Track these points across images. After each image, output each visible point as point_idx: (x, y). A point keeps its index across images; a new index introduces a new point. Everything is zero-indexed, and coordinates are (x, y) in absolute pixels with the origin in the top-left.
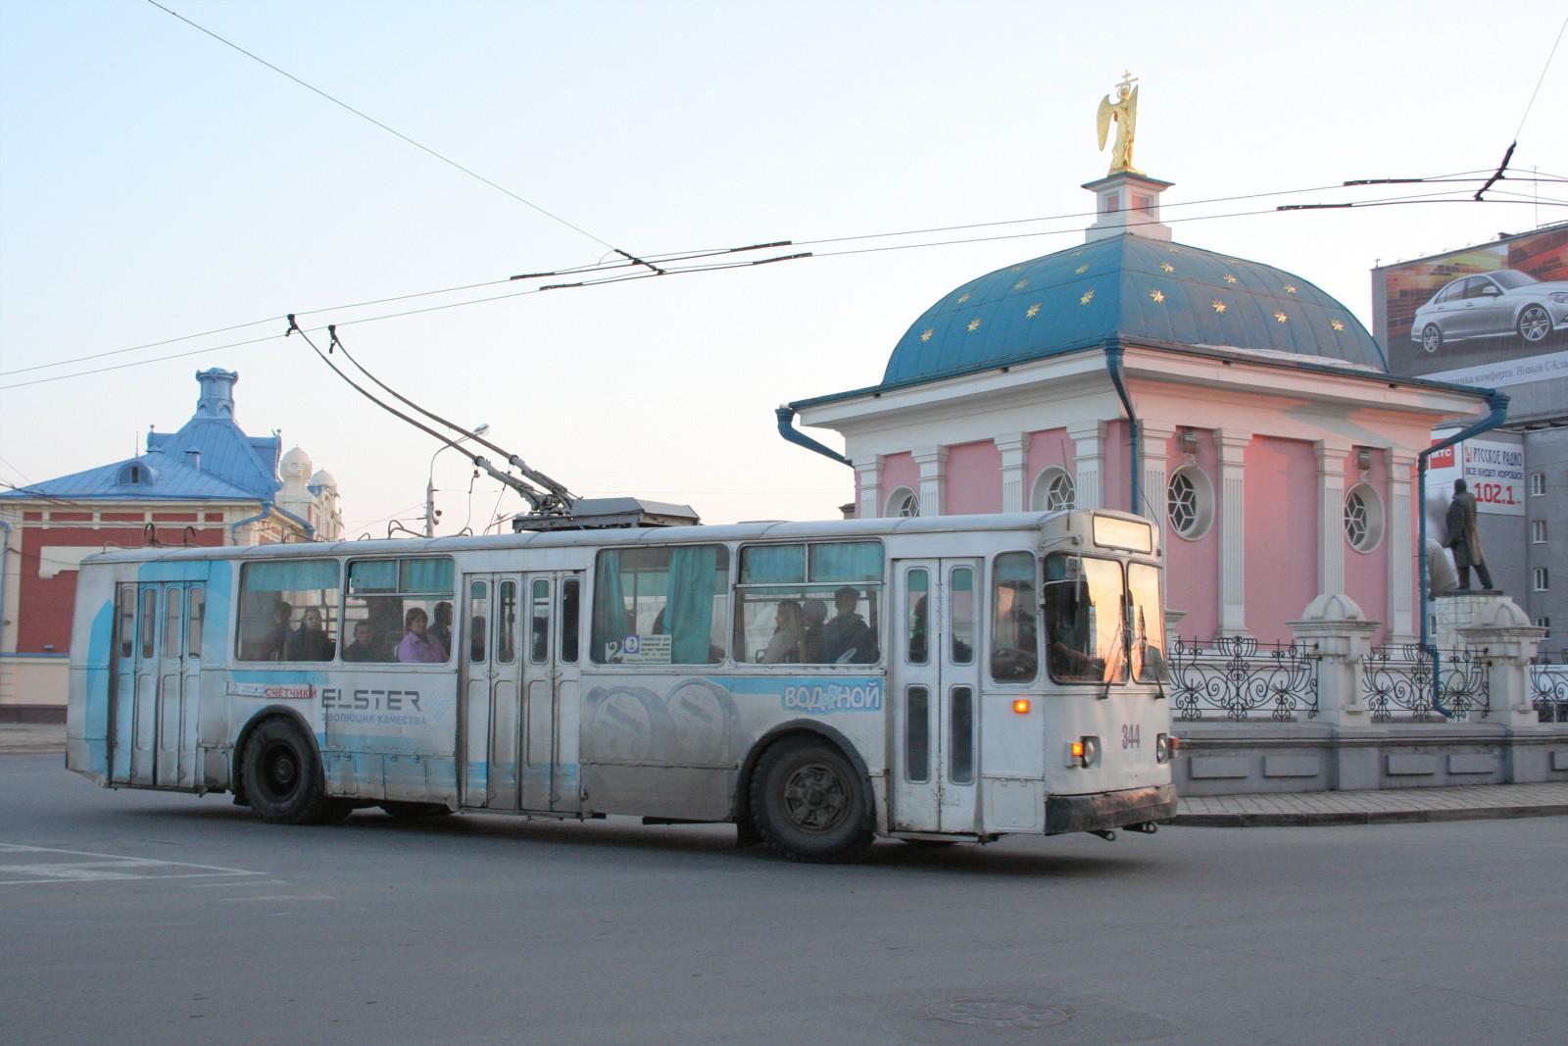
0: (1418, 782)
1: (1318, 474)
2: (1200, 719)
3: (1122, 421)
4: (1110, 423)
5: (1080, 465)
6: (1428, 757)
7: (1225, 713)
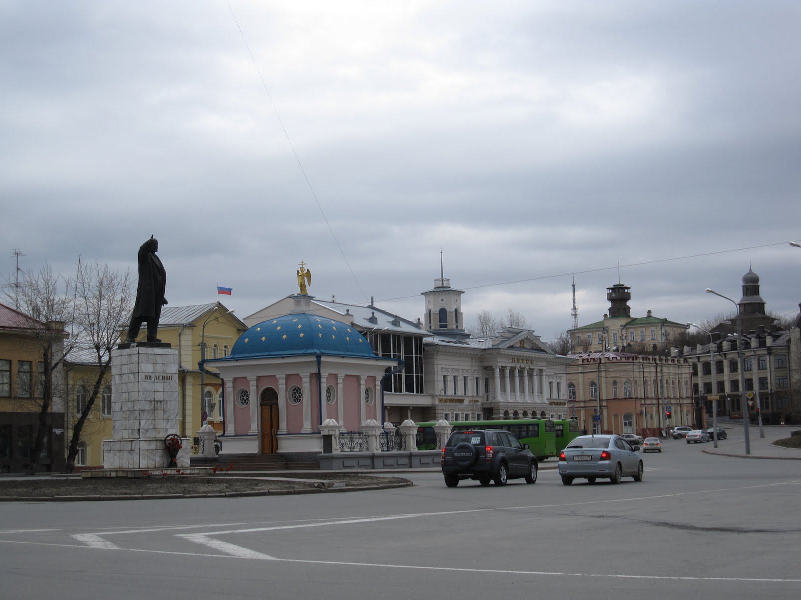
0: (391, 466)
1: (359, 385)
2: (344, 451)
3: (316, 374)
4: (312, 374)
5: (303, 385)
6: (116, 465)
7: (349, 450)
